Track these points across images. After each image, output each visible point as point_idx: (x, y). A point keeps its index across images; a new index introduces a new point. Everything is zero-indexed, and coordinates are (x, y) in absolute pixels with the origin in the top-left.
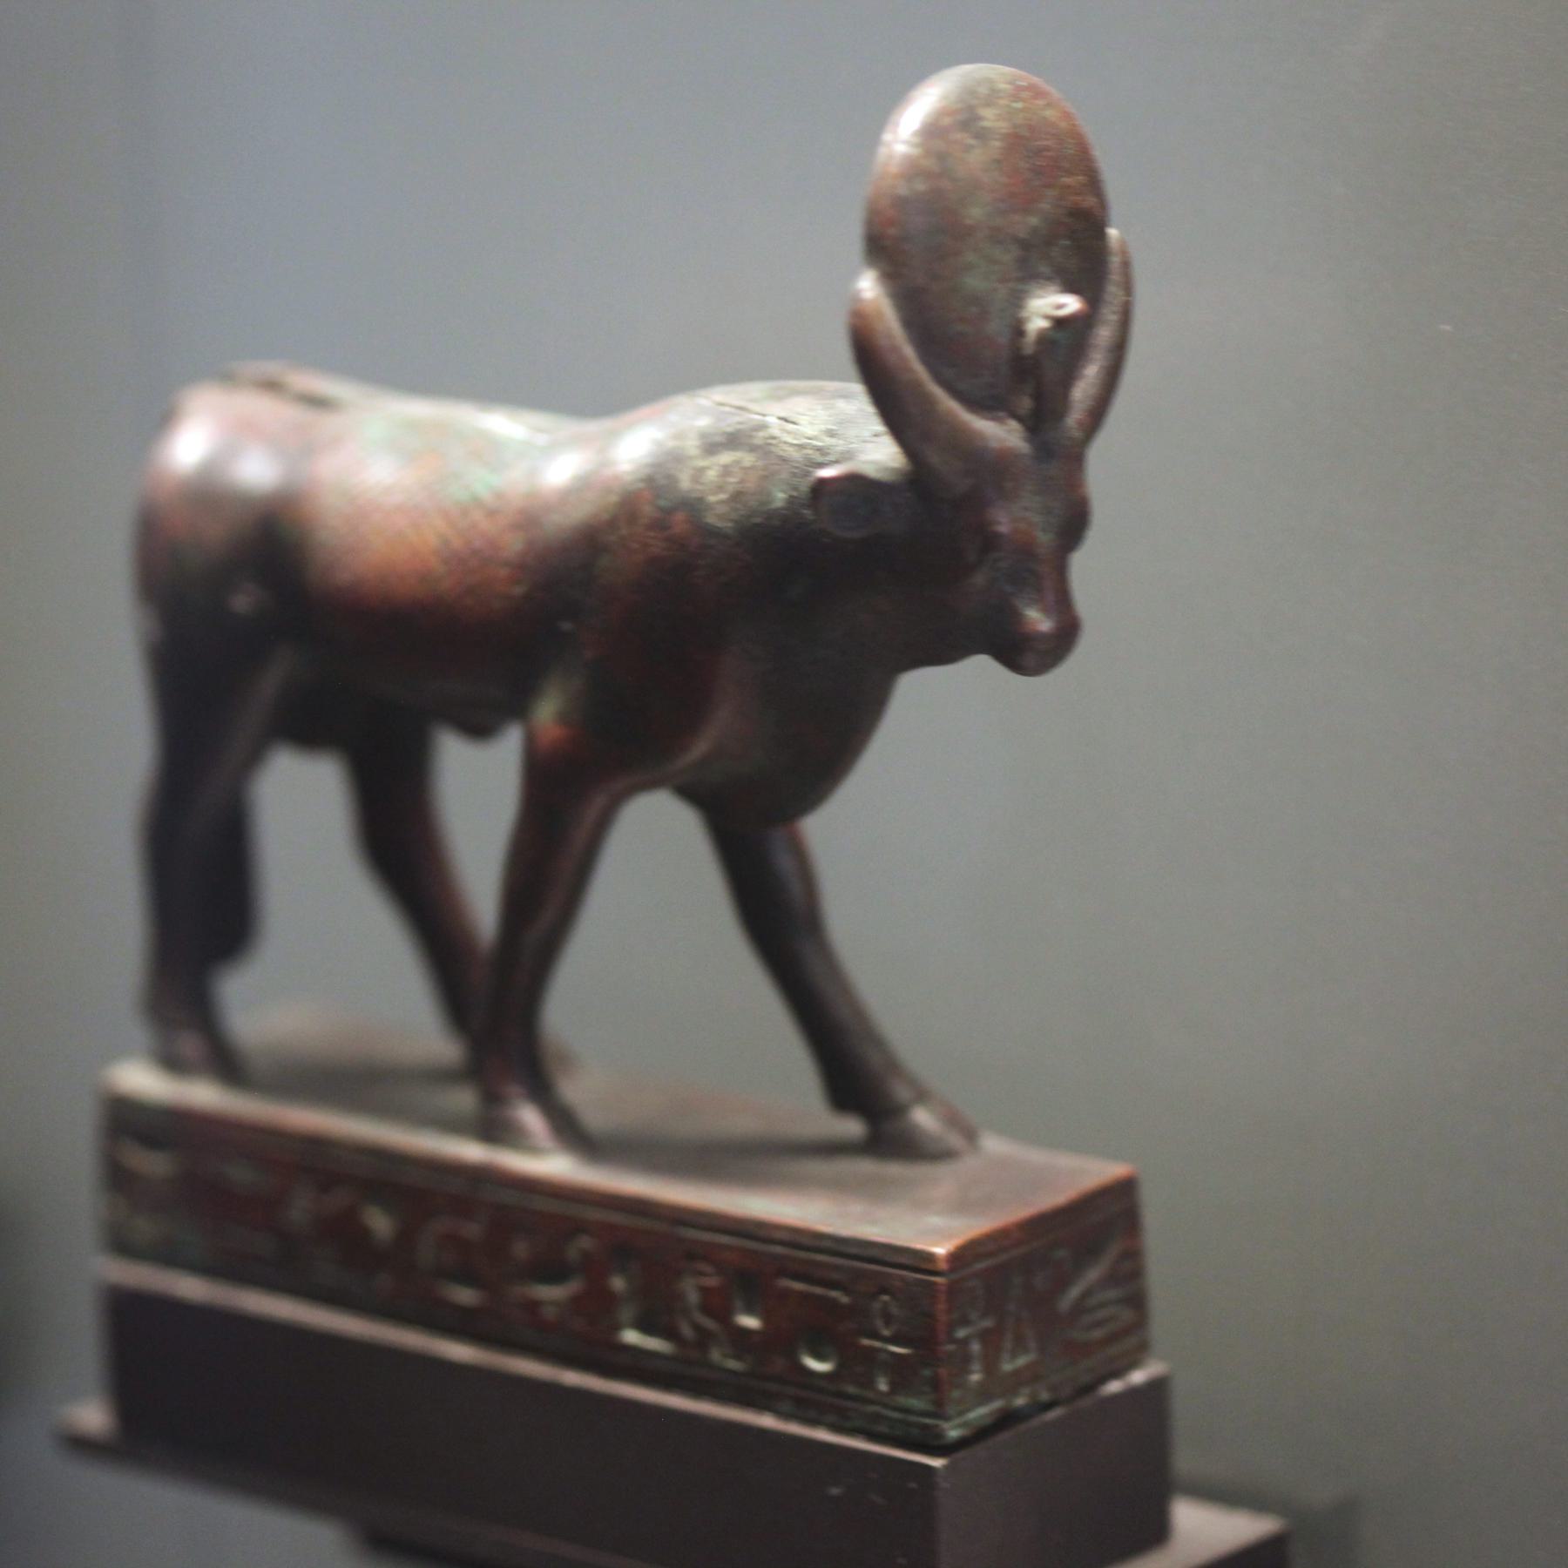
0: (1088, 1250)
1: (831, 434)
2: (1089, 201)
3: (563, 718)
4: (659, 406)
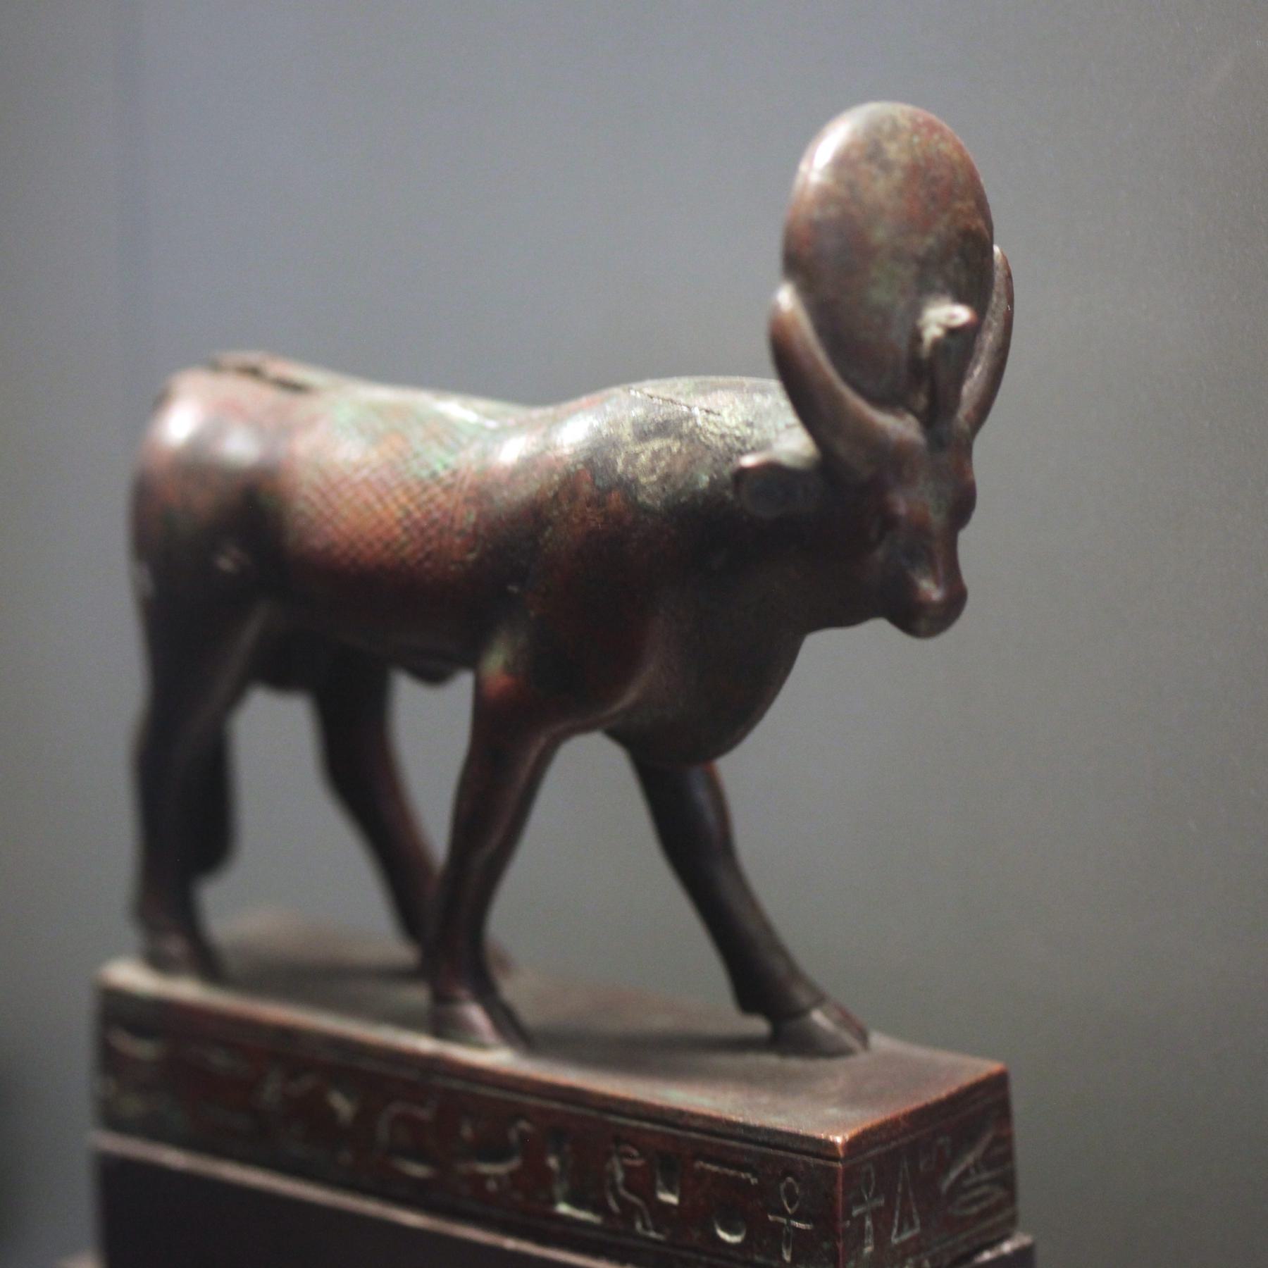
0: (965, 1137)
1: (750, 425)
2: (980, 223)
3: (509, 668)
4: (597, 396)
